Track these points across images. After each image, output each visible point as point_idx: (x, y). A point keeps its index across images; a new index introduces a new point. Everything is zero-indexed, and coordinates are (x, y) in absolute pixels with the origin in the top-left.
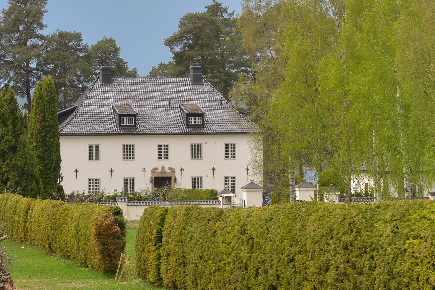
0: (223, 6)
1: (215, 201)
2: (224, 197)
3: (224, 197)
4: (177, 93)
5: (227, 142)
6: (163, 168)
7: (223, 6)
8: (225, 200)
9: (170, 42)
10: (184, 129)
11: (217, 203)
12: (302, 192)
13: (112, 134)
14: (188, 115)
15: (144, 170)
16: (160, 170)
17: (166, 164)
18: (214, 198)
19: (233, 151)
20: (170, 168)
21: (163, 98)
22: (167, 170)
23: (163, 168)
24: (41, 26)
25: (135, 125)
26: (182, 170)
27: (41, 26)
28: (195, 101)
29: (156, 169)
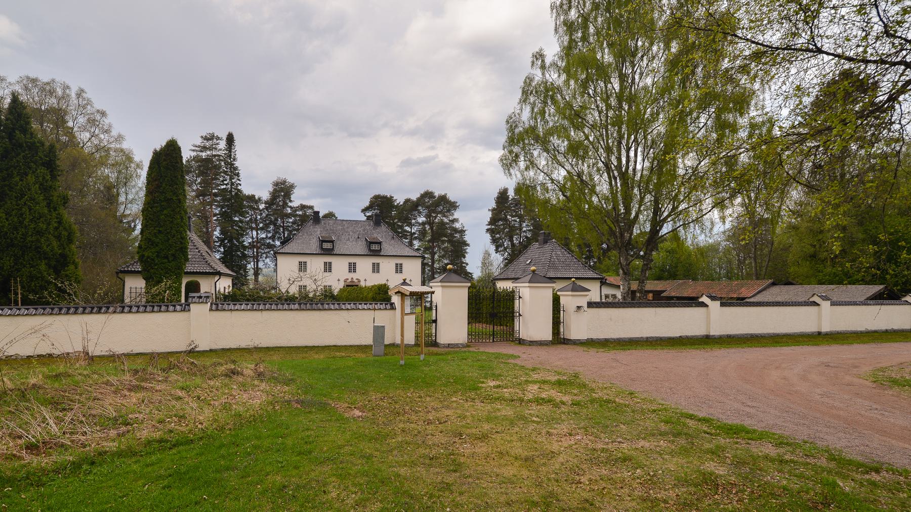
0: (395, 198)
1: (386, 304)
2: (408, 293)
3: (408, 293)
4: (364, 230)
5: (397, 262)
6: (352, 279)
7: (395, 198)
8: (408, 302)
9: (364, 211)
10: (365, 252)
11: (388, 306)
12: (534, 290)
13: (315, 254)
14: (371, 243)
15: (339, 280)
16: (350, 280)
17: (354, 276)
18: (384, 299)
19: (401, 268)
20: (357, 279)
21: (354, 233)
22: (355, 280)
23: (352, 279)
24: (291, 201)
25: (333, 249)
26: (365, 280)
27: (291, 201)
28: (375, 236)
29: (348, 279)
